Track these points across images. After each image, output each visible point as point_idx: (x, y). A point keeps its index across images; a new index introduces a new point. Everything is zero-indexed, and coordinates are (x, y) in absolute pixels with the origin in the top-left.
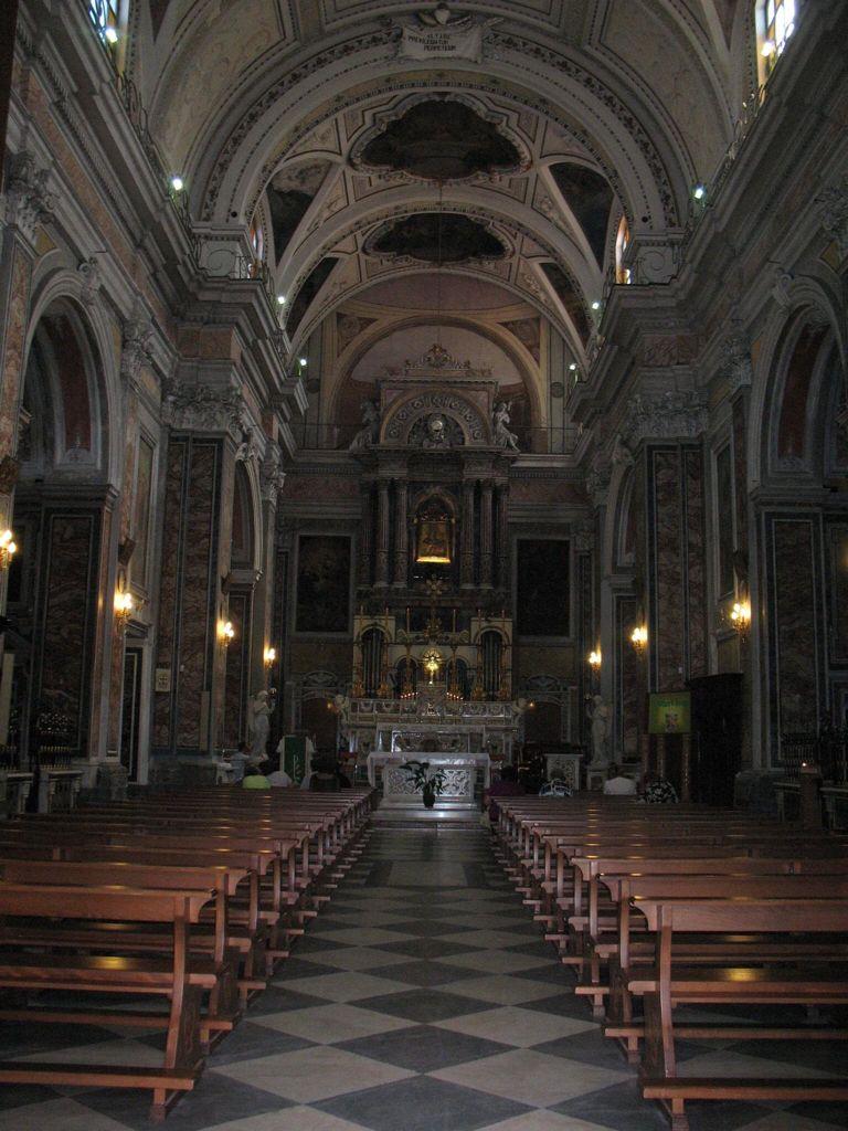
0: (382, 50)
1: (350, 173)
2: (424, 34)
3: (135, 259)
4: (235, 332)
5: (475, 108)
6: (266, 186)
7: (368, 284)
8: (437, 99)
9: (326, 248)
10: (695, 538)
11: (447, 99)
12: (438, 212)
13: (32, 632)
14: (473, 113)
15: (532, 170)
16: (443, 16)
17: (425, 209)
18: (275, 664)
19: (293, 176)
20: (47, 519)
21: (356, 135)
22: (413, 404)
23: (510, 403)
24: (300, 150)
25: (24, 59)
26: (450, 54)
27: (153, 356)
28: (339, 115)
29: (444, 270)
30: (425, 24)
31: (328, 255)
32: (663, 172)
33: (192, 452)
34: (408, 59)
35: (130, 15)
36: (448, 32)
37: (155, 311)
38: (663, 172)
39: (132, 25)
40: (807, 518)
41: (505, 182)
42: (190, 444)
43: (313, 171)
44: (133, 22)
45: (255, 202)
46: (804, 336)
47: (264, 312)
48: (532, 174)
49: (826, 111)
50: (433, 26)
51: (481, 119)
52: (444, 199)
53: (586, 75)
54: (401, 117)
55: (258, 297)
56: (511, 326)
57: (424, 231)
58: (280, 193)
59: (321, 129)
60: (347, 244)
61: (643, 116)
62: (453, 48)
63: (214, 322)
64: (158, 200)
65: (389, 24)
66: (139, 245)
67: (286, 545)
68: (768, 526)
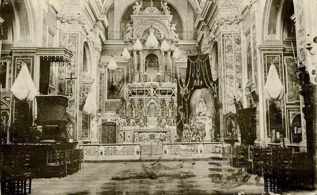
10: (238, 64)
13: (10, 99)
18: (288, 180)
20: (14, 60)
22: (144, 24)
23: (176, 24)
33: (68, 38)
40: (278, 55)
42: (68, 35)
67: (103, 71)
68: (264, 58)
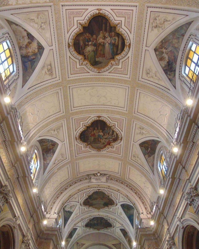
0: (87, 181)
1: (81, 207)
2: (96, 177)
3: (30, 220)
4: (52, 242)
5: (105, 193)
6: (63, 208)
7: (84, 235)
8: (98, 191)
9: (75, 225)
11: (100, 191)
12: (98, 217)
14: (105, 194)
15: (117, 206)
16: (99, 174)
17: (96, 216)
19: (69, 208)
21: (82, 198)
24: (71, 201)
25: (12, 167)
26: (100, 181)
27: (30, 246)
28: (79, 194)
29: (100, 232)
30: (96, 176)
31: (75, 227)
32: (144, 203)
34: (92, 182)
35: (39, 169)
36: (100, 177)
37: (32, 234)
38: (144, 203)
39: (38, 172)
41: (112, 209)
43: (73, 206)
44: (40, 169)
45: (60, 211)
46: (188, 236)
47: (59, 236)
48: (117, 207)
49: (194, 141)
50: (97, 176)
51: (106, 195)
52: (100, 213)
53: (126, 185)
54: (91, 195)
55: (58, 233)
56: (114, 245)
57: (95, 222)
58: (66, 211)
59: (76, 196)
60: (79, 224)
61: (138, 192)
62: (101, 180)
63: (47, 239)
64: (38, 206)
65: (89, 176)
66: (32, 217)
